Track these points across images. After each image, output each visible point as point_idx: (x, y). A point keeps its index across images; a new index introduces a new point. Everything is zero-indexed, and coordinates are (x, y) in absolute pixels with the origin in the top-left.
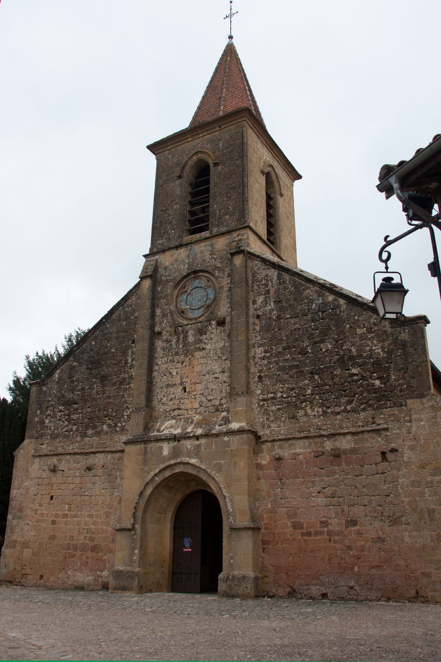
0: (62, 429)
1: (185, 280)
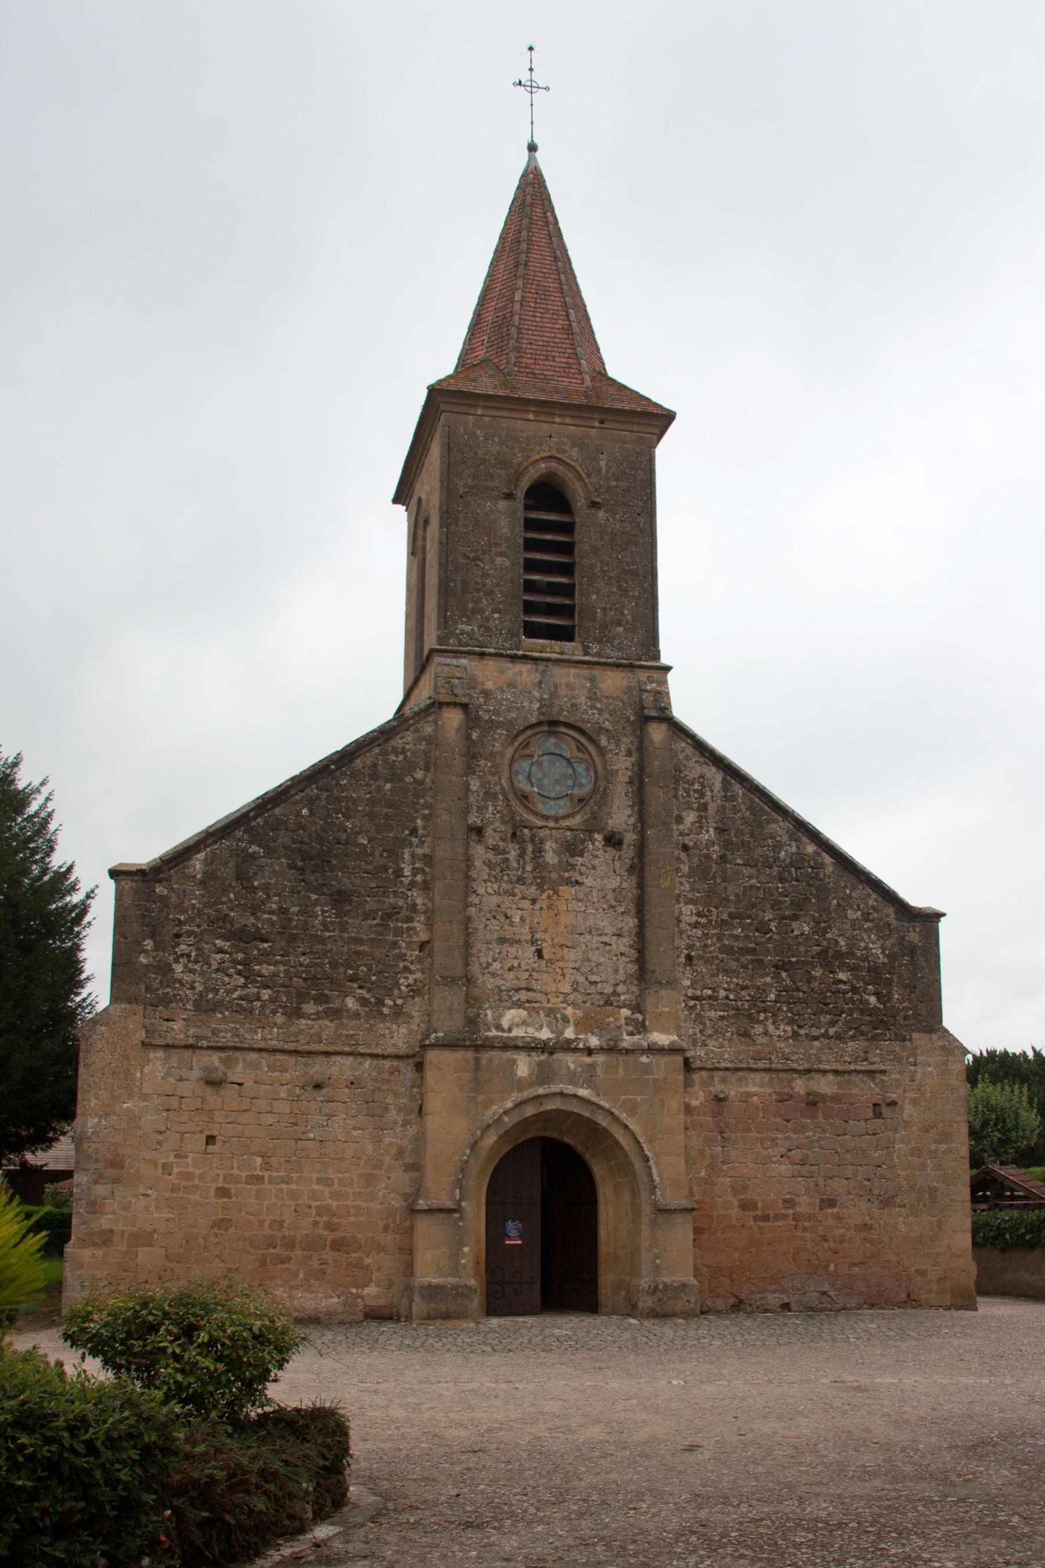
0: (229, 992)
1: (529, 733)
